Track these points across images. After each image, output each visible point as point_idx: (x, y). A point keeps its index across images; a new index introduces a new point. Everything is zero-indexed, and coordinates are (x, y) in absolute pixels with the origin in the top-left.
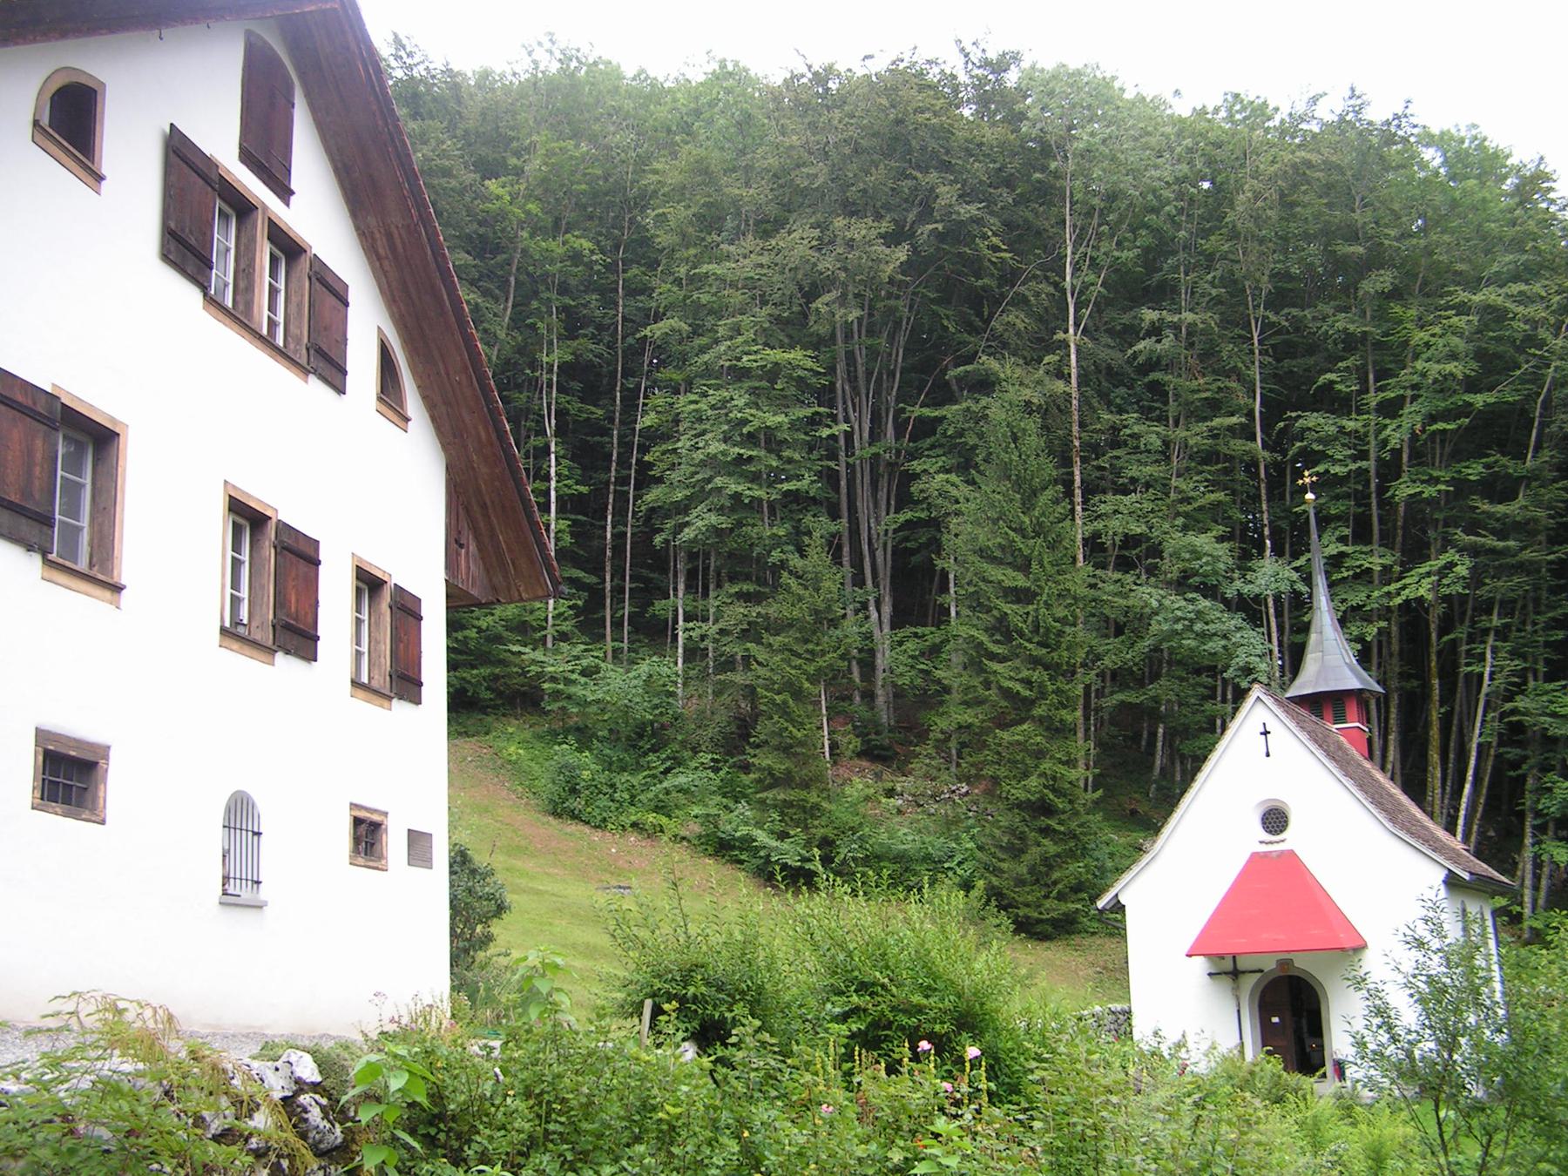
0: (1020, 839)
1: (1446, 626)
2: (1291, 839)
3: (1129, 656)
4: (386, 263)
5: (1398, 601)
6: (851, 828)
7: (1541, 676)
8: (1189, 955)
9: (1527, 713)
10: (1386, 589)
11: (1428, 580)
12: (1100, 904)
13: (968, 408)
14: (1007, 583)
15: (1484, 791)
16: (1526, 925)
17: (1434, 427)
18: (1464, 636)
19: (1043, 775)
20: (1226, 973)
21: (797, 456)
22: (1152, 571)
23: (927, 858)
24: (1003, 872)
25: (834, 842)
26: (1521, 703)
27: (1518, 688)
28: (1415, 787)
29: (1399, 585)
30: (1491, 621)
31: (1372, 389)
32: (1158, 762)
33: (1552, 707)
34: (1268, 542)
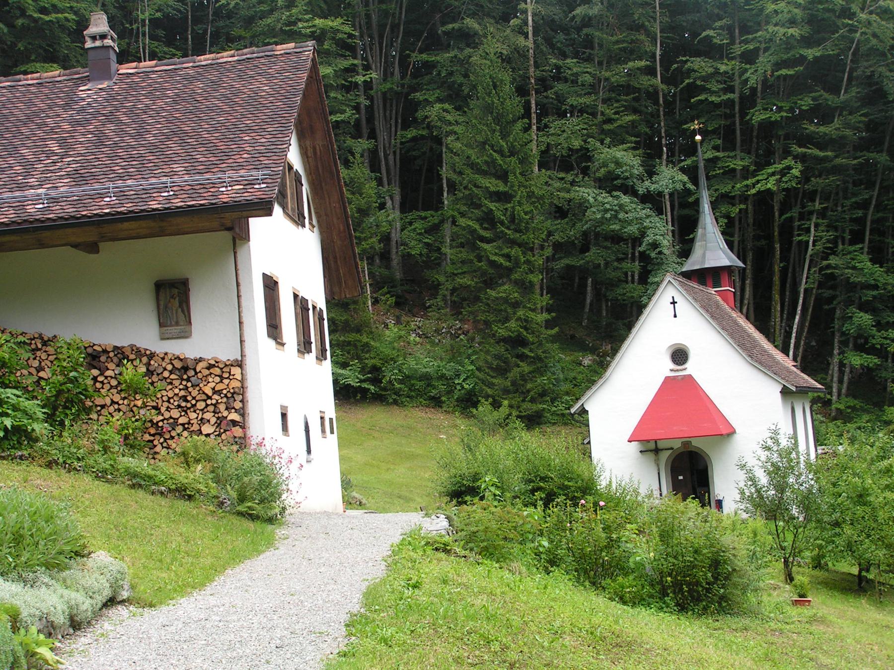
0: (504, 362)
1: (785, 206)
2: (691, 368)
3: (572, 233)
4: (310, 160)
5: (753, 191)
6: (392, 359)
7: (847, 241)
8: (630, 441)
9: (836, 267)
10: (745, 183)
11: (774, 178)
12: (573, 411)
13: (456, 56)
14: (492, 189)
15: (809, 317)
16: (833, 406)
17: (780, 72)
18: (796, 215)
19: (519, 319)
20: (651, 451)
21: (340, 97)
22: (585, 171)
23: (442, 377)
24: (493, 384)
25: (380, 368)
26: (833, 260)
27: (831, 251)
28: (763, 323)
29: (754, 180)
30: (814, 206)
31: (737, 41)
32: (588, 301)
33: (853, 263)
34: (665, 149)
